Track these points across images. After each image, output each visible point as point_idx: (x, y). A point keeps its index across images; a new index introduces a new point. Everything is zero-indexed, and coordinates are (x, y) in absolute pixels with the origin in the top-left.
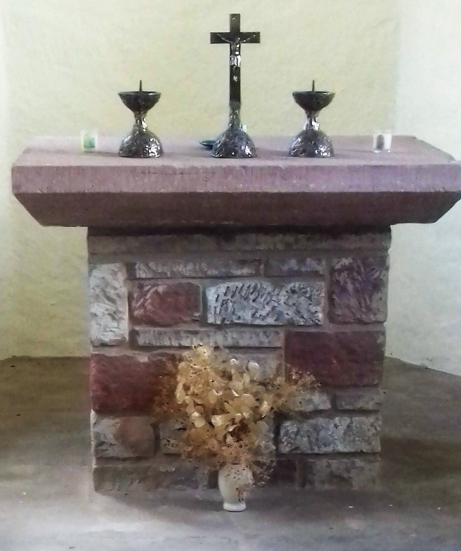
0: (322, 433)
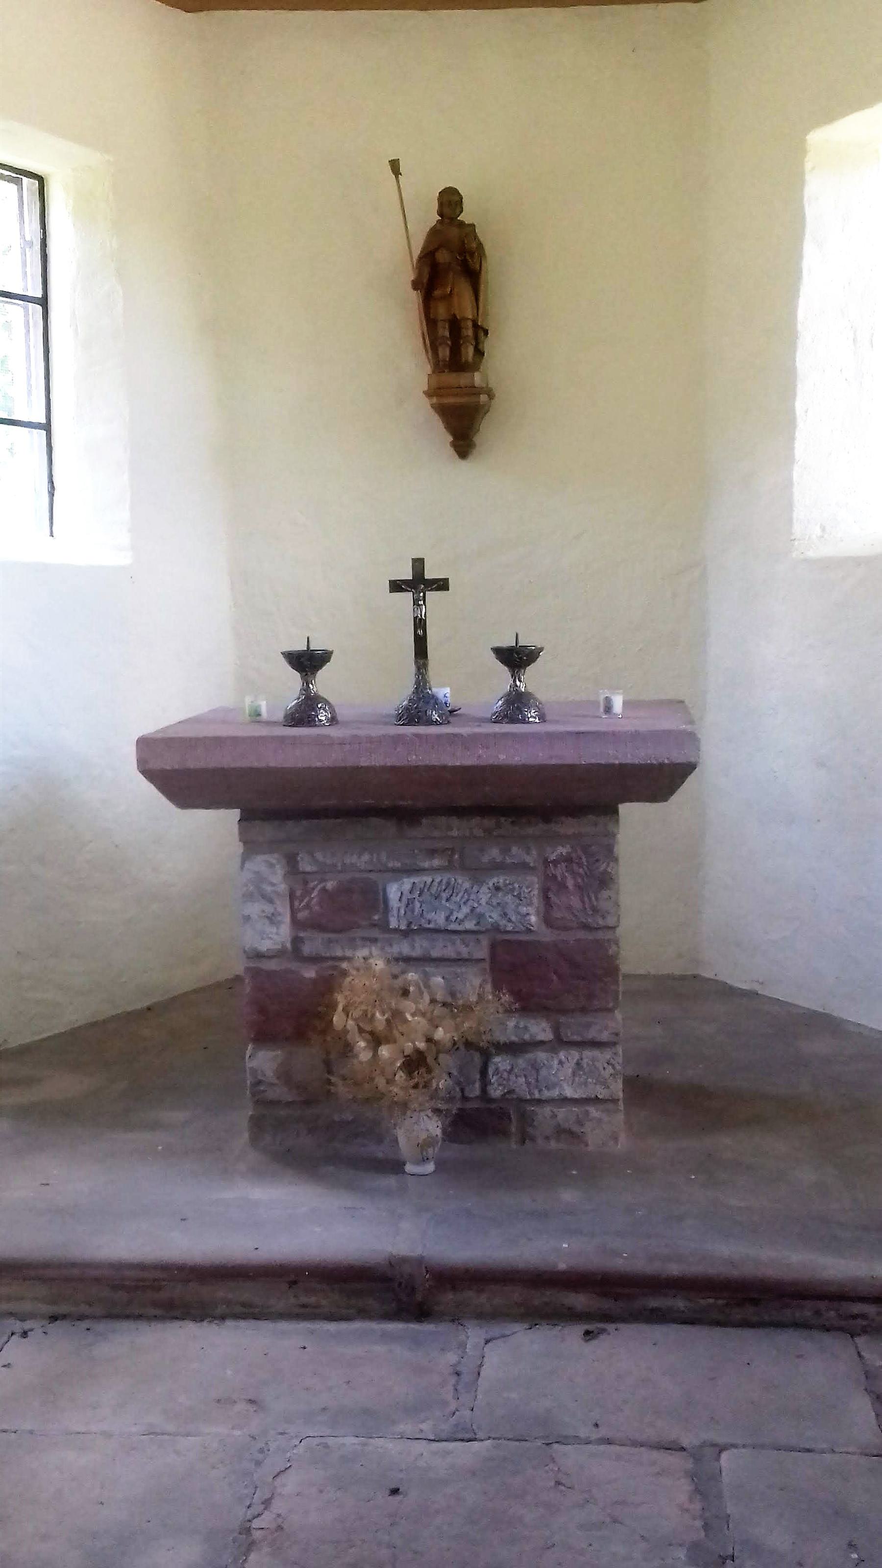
0: (543, 1072)
